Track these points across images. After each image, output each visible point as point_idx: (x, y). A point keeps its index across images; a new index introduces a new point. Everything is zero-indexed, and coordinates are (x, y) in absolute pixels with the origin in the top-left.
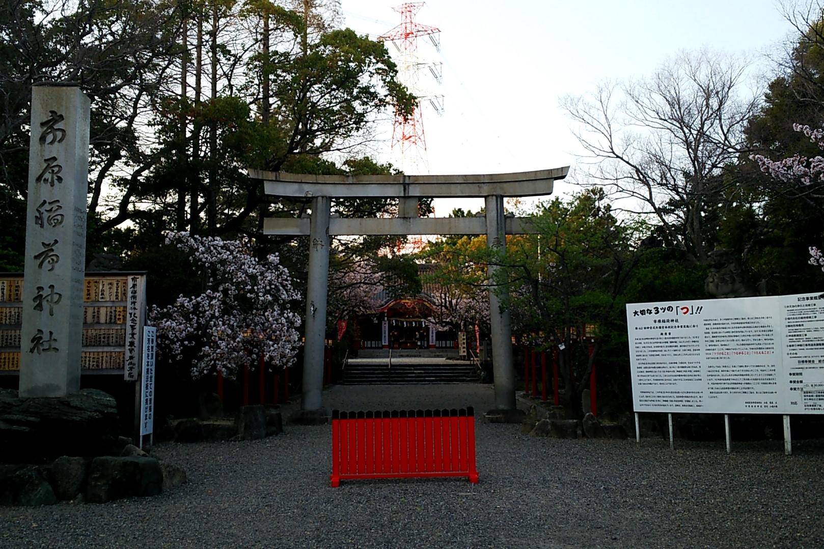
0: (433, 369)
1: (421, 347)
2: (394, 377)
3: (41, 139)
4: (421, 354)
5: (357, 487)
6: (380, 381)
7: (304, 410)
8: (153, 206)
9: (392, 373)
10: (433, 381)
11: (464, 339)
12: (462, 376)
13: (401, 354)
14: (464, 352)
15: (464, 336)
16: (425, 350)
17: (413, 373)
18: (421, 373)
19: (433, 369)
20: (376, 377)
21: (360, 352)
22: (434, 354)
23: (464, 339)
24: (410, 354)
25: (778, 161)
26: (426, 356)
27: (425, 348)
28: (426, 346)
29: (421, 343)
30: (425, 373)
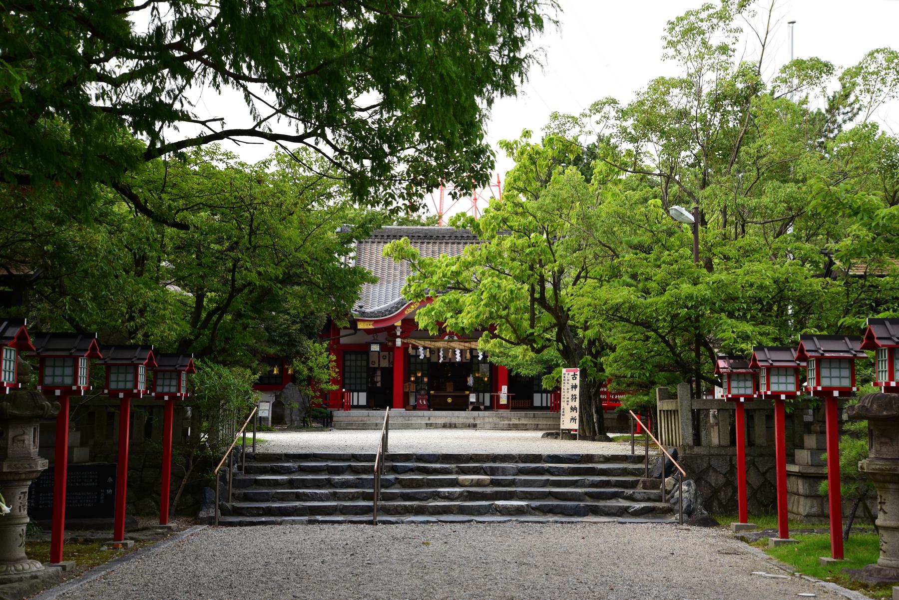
0: (521, 472)
1: (476, 408)
2: (392, 497)
3: (596, 104)
4: (478, 422)
5: (347, 138)
6: (344, 511)
7: (827, 495)
8: (731, 74)
9: (388, 484)
10: (519, 511)
11: (574, 387)
12: (614, 496)
13: (432, 421)
14: (573, 419)
15: (574, 377)
16: (487, 413)
17: (455, 483)
18: (479, 484)
19: (521, 472)
20: (334, 496)
21: (339, 415)
22: (506, 422)
23: (574, 387)
24: (454, 421)
25: (239, 480)
26: (488, 426)
27: (487, 409)
28: (487, 403)
29: (478, 398)
30: (494, 483)
